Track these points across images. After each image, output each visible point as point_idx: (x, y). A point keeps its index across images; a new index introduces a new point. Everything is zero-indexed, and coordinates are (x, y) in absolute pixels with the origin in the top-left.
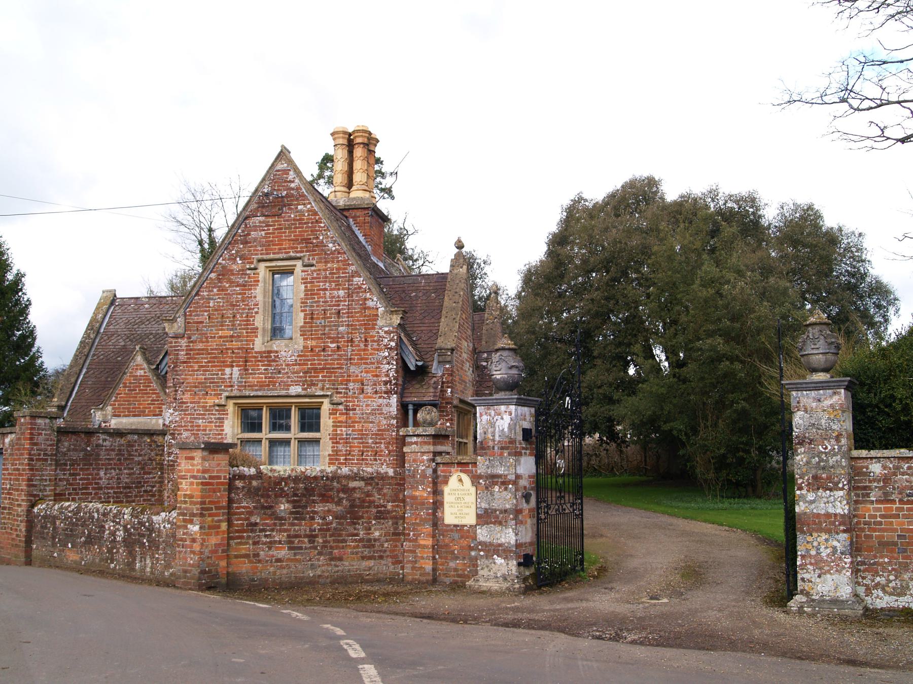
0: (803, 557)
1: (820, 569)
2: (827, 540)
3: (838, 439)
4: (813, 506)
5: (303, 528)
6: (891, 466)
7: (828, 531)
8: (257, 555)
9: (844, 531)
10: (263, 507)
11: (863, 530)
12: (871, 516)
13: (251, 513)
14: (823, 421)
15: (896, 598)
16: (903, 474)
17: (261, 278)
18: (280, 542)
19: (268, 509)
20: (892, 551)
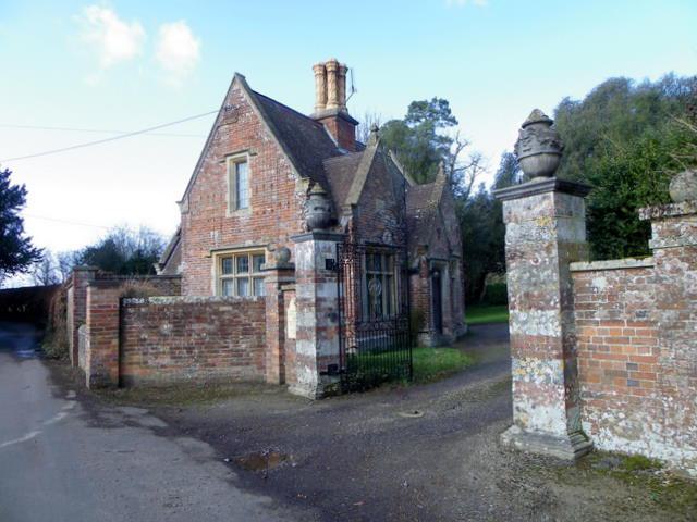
0: (517, 383)
1: (534, 398)
2: (540, 366)
3: (548, 250)
4: (525, 327)
5: (182, 342)
6: (617, 279)
7: (541, 357)
8: (146, 363)
9: (558, 357)
10: (150, 327)
11: (587, 355)
12: (595, 340)
13: (140, 332)
14: (534, 231)
15: (626, 441)
16: (632, 289)
17: (228, 167)
18: (164, 353)
19: (154, 328)
20: (621, 383)
